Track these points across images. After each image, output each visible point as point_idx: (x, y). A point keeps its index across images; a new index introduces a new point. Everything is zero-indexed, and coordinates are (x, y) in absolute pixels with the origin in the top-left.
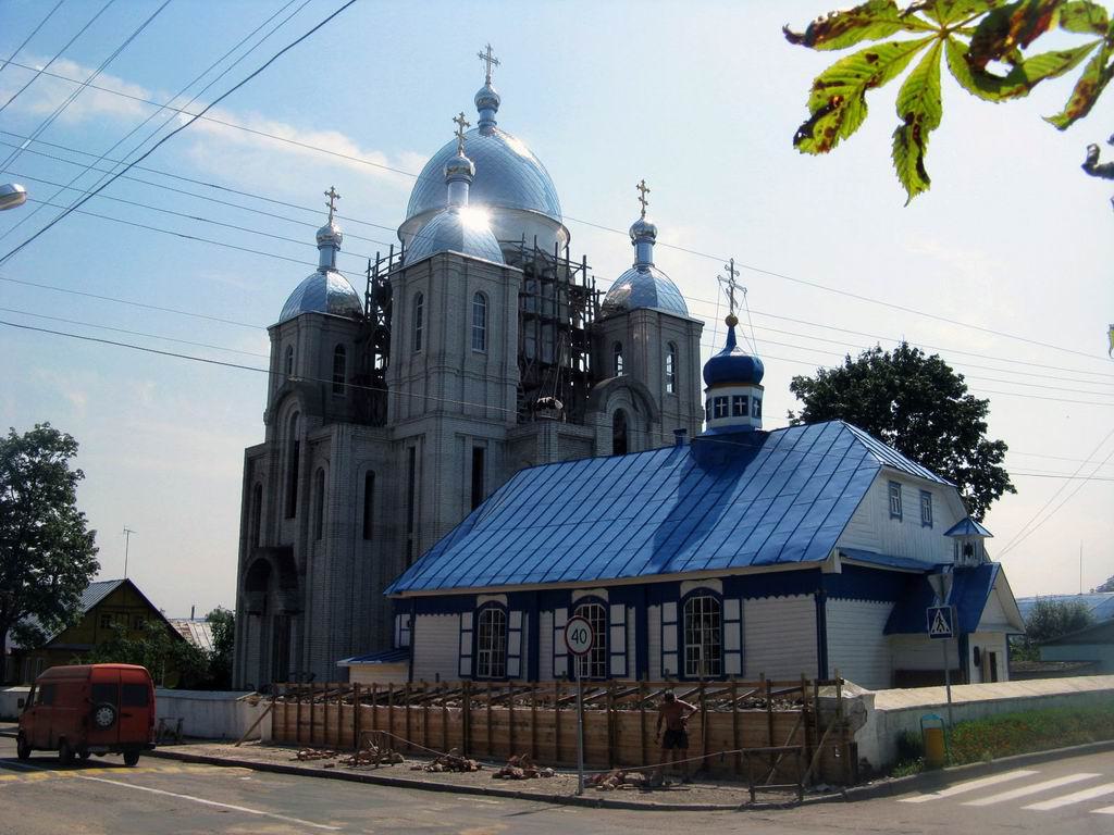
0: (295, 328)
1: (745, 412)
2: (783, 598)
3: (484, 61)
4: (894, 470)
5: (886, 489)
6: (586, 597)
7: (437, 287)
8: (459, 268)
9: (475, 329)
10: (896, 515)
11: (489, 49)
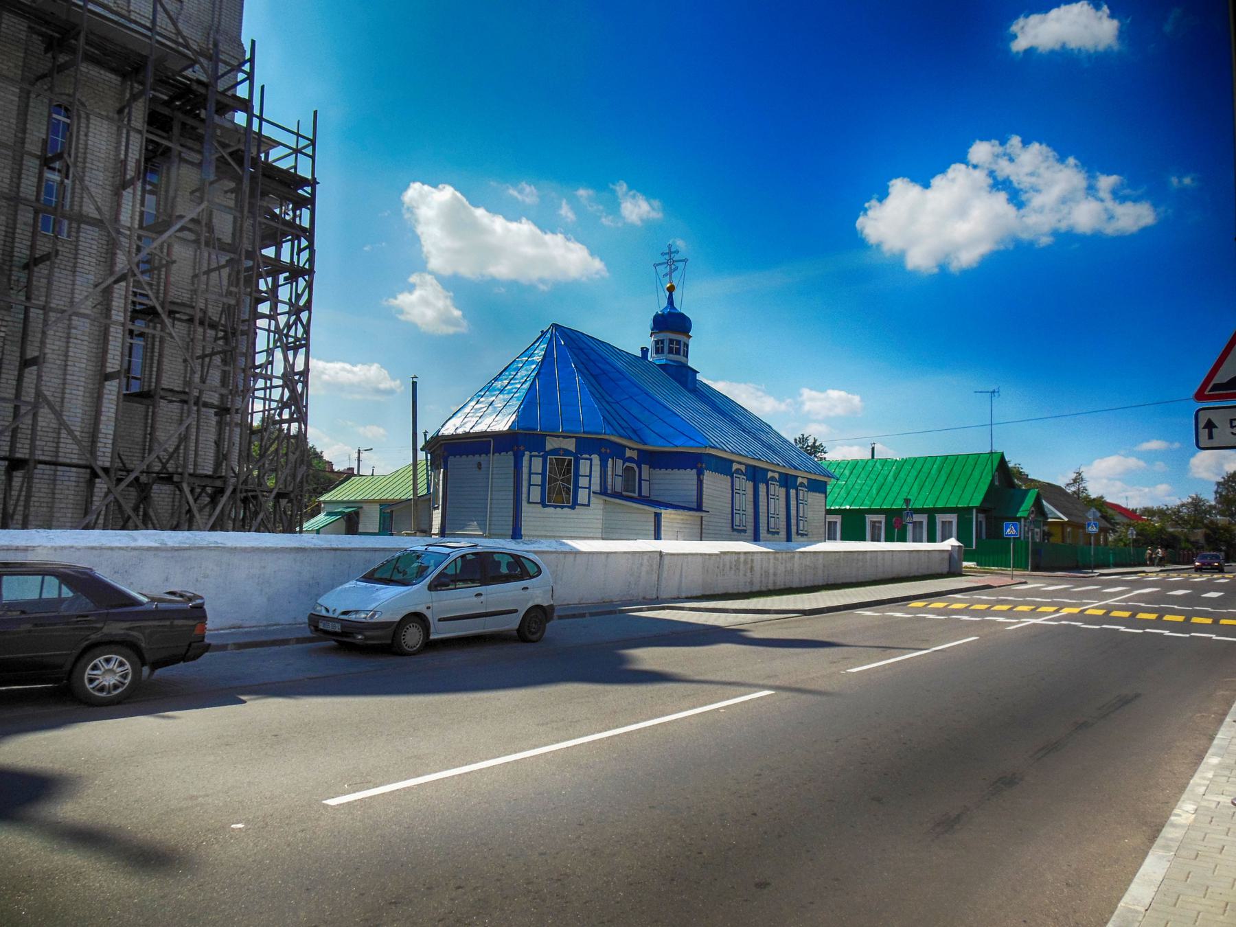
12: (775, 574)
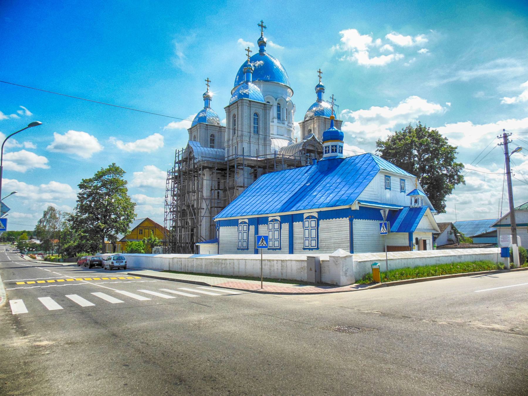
0: (196, 129)
1: (336, 151)
2: (345, 218)
3: (260, 28)
4: (387, 171)
5: (384, 178)
6: (273, 219)
7: (240, 113)
8: (247, 105)
9: (254, 126)
10: (388, 187)
11: (262, 22)
12: (188, 266)
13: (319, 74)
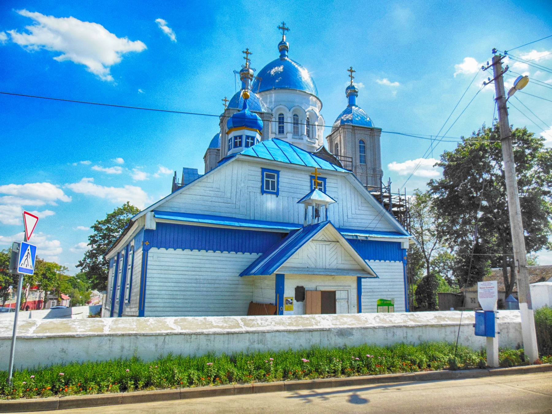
13: (349, 73)
